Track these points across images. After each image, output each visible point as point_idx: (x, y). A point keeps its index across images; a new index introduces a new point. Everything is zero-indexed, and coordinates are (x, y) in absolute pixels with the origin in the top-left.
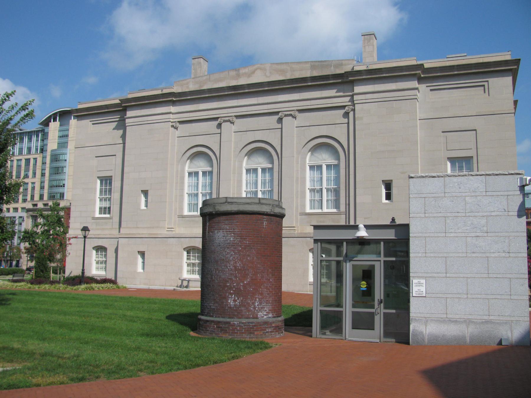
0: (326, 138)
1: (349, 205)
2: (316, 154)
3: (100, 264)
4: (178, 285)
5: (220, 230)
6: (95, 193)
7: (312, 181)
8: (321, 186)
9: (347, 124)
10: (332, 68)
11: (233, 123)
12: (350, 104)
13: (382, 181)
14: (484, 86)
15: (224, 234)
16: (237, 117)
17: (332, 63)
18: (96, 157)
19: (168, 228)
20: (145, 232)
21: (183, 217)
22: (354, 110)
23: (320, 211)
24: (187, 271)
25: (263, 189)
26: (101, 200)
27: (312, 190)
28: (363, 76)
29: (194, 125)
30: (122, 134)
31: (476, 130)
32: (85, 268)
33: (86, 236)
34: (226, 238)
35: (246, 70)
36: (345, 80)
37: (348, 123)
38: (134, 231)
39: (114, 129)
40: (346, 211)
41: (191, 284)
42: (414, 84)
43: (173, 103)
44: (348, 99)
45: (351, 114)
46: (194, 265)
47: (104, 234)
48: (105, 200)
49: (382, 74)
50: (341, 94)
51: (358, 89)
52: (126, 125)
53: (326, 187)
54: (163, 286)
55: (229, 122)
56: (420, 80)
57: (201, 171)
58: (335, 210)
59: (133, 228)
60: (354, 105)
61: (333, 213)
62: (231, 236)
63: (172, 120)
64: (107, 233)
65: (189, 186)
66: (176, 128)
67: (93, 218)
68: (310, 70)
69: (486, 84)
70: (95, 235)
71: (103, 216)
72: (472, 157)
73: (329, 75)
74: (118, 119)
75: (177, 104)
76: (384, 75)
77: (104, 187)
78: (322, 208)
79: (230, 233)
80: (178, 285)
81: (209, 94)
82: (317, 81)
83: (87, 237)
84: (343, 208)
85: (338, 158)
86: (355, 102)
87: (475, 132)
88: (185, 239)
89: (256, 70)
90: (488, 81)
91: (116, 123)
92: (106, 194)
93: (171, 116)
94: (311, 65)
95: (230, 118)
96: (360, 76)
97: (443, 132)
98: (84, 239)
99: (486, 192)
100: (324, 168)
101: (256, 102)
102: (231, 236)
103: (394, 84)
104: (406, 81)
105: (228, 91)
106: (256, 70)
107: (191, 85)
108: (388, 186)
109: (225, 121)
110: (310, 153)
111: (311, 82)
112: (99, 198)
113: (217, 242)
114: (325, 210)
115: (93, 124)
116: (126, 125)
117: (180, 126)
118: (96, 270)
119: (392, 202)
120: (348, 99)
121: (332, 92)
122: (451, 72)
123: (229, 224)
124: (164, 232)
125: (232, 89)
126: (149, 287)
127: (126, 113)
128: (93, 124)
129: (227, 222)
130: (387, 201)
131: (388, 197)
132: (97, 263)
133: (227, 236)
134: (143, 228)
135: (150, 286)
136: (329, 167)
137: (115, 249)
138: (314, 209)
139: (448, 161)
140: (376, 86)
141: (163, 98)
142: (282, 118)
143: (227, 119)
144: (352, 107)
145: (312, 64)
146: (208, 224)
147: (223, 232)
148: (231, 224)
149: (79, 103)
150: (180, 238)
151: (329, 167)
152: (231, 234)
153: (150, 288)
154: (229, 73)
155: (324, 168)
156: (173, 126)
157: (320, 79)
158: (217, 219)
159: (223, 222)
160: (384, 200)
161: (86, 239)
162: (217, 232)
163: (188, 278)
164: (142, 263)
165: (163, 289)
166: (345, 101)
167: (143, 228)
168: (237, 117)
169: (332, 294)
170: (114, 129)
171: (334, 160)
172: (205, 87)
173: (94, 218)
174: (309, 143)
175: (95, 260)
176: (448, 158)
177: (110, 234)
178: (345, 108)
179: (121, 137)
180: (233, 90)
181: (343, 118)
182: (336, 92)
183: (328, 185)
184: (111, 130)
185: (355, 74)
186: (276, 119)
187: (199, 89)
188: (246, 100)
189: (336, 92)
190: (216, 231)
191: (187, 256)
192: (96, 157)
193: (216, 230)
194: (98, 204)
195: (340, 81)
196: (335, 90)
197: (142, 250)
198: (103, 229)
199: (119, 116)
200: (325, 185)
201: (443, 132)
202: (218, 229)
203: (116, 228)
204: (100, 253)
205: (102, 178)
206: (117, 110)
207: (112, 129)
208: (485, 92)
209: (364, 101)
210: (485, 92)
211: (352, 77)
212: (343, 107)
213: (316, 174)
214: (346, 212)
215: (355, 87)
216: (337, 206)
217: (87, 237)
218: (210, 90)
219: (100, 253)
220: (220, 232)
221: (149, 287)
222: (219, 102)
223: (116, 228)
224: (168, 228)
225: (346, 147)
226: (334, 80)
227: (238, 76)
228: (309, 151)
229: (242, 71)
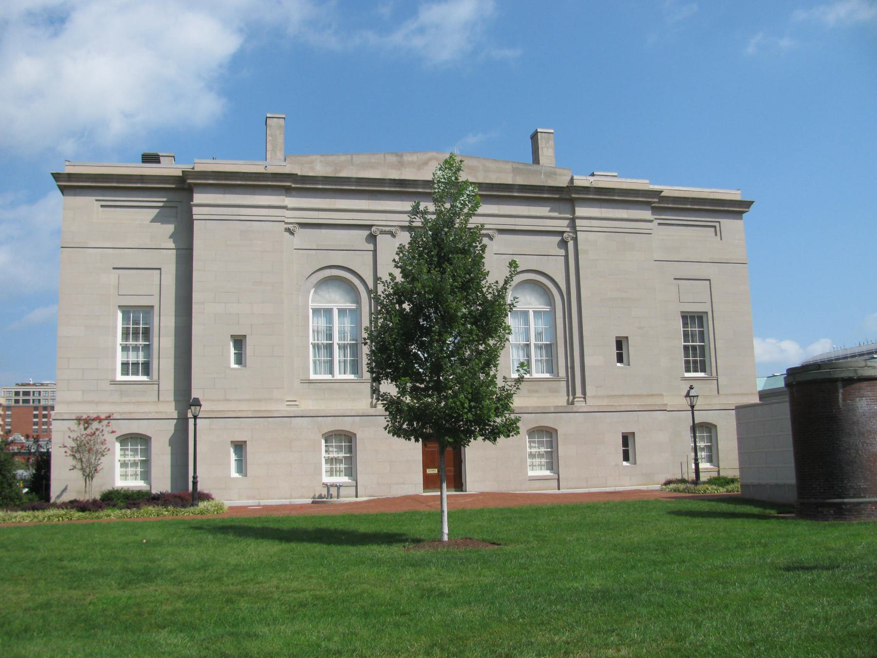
0: (322, 270)
1: (573, 368)
2: (321, 293)
3: (131, 467)
4: (315, 495)
5: (863, 397)
6: (115, 336)
7: (317, 332)
8: (331, 341)
9: (372, 252)
10: (543, 176)
11: (393, 235)
12: (568, 229)
13: (231, 336)
14: (715, 227)
15: (868, 402)
16: (501, 231)
17: (542, 169)
18: (114, 268)
19: (287, 401)
20: (245, 408)
21: (311, 382)
22: (575, 240)
23: (329, 377)
24: (121, 475)
25: (523, 343)
26: (125, 348)
27: (317, 347)
28: (589, 194)
29: (324, 231)
30: (173, 232)
31: (709, 280)
32: (198, 474)
33: (197, 416)
34: (870, 407)
35: (414, 158)
36: (564, 196)
37: (566, 257)
38: (263, 407)
39: (153, 221)
40: (567, 376)
41: (343, 491)
42: (647, 214)
43: (288, 191)
44: (566, 222)
45: (571, 244)
46: (337, 460)
47: (144, 413)
48: (136, 348)
49: (613, 196)
50: (556, 214)
51: (580, 211)
52: (194, 218)
53: (339, 342)
54: (285, 498)
55: (389, 234)
56: (655, 210)
57: (337, 309)
58: (547, 376)
59: (218, 400)
60: (576, 232)
61: (541, 380)
62: (874, 404)
63: (286, 220)
64: (150, 409)
65: (313, 331)
66: (292, 233)
67: (111, 383)
68: (512, 175)
69: (717, 225)
70: (121, 413)
71: (131, 378)
72: (153, 307)
73: (545, 186)
74: (161, 204)
75: (294, 193)
76: (616, 198)
77: (131, 326)
78: (331, 372)
79: (873, 401)
80: (315, 495)
81: (356, 185)
82: (526, 192)
83: (199, 416)
84: (562, 373)
85: (551, 301)
86: (578, 229)
87: (159, 271)
88: (325, 418)
89: (430, 159)
90: (719, 222)
91: (157, 210)
92: (136, 338)
93: (288, 213)
94: (513, 167)
95: (393, 229)
96: (587, 194)
97: (675, 279)
98: (193, 420)
99: (254, 356)
100: (531, 314)
101: (526, 213)
102: (874, 404)
103: (625, 211)
104: (638, 209)
105: (389, 187)
106: (430, 159)
107: (318, 166)
108: (239, 342)
109: (382, 232)
110: (313, 289)
111: (518, 192)
112: (121, 344)
113: (860, 411)
114: (338, 376)
115: (102, 206)
116: (194, 218)
117: (300, 232)
118: (121, 479)
119: (245, 366)
120: (566, 222)
121: (544, 211)
122: (683, 204)
123: (872, 391)
124: (283, 408)
125: (398, 184)
126: (259, 502)
127: (193, 195)
128: (102, 206)
129: (869, 388)
130: (237, 366)
131: (240, 360)
132: (124, 465)
133: (871, 404)
134: (239, 400)
135: (261, 501)
136: (342, 312)
137: (169, 439)
138: (320, 374)
139: (119, 311)
140: (603, 210)
141: (272, 181)
142: (377, 235)
143: (387, 229)
144: (571, 234)
145: (515, 166)
146: (841, 391)
147: (866, 399)
148: (874, 391)
149: (67, 163)
150: (316, 418)
151: (342, 312)
152: (874, 402)
153: (292, 503)
154: (385, 157)
155: (531, 314)
156: (289, 229)
157: (531, 189)
158: (857, 385)
159: (865, 389)
160: (233, 365)
161: (198, 421)
162: (859, 400)
163: (330, 483)
164: (236, 462)
165: (587, 491)
166: (562, 225)
167: (239, 400)
168: (501, 231)
169: (561, 490)
170: (153, 221)
171: (349, 302)
172: (344, 174)
173: (114, 383)
174: (314, 275)
175: (119, 461)
176: (119, 306)
177: (156, 412)
178: (371, 228)
179: (171, 237)
180: (398, 185)
181: (558, 248)
182: (550, 211)
183: (343, 338)
184: (148, 222)
185: (580, 190)
186: (365, 237)
187: (333, 175)
188: (382, 202)
189: (550, 211)
190: (858, 399)
191: (121, 449)
192: (114, 268)
193: (857, 397)
194: (120, 357)
195: (557, 196)
196: (548, 209)
197: (239, 438)
198: (139, 403)
199: (165, 199)
200: (336, 340)
201: (675, 279)
202: (860, 397)
203: (168, 402)
204: (129, 447)
205: (126, 309)
206: (89, 186)
207: (150, 220)
208: (716, 235)
209: (589, 229)
210: (716, 235)
211: (576, 193)
212: (561, 233)
213: (322, 323)
214: (568, 378)
215: (576, 208)
216: (551, 370)
217: (199, 416)
218: (326, 179)
219: (129, 447)
220: (862, 400)
221: (259, 502)
222: (370, 201)
223: (168, 402)
224: (287, 401)
225: (564, 288)
226: (549, 193)
227: (401, 165)
228: (313, 288)
229: (408, 158)
